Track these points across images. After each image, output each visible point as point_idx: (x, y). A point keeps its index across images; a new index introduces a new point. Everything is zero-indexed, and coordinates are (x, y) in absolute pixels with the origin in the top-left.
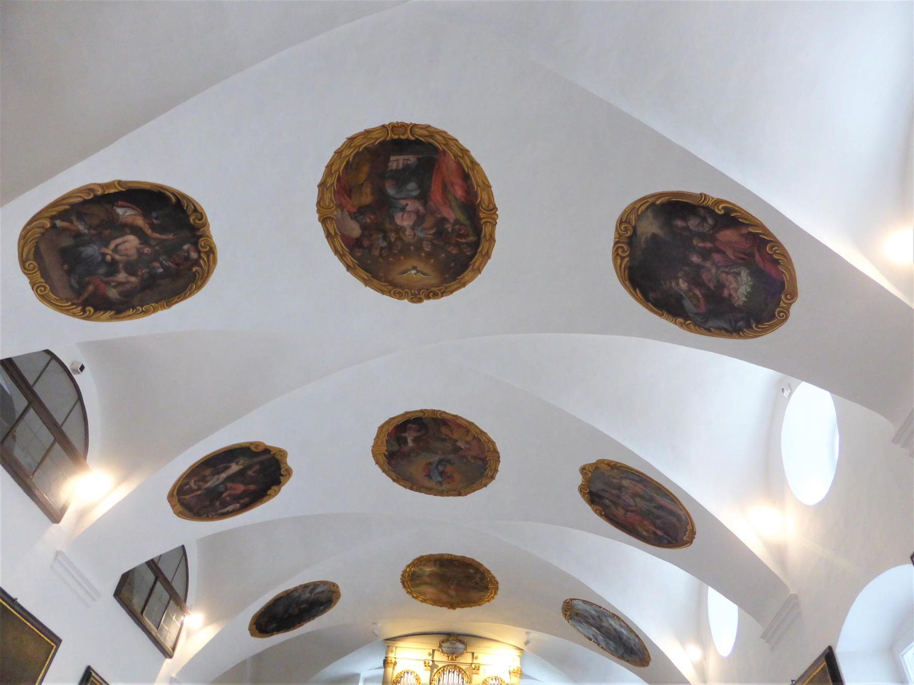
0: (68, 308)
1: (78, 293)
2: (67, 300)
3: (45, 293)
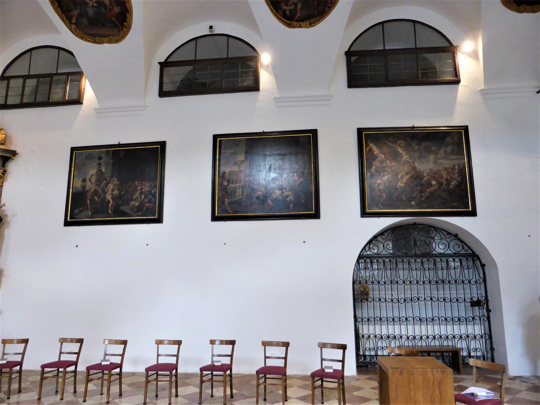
0: (124, 32)
1: (115, 26)
2: (119, 31)
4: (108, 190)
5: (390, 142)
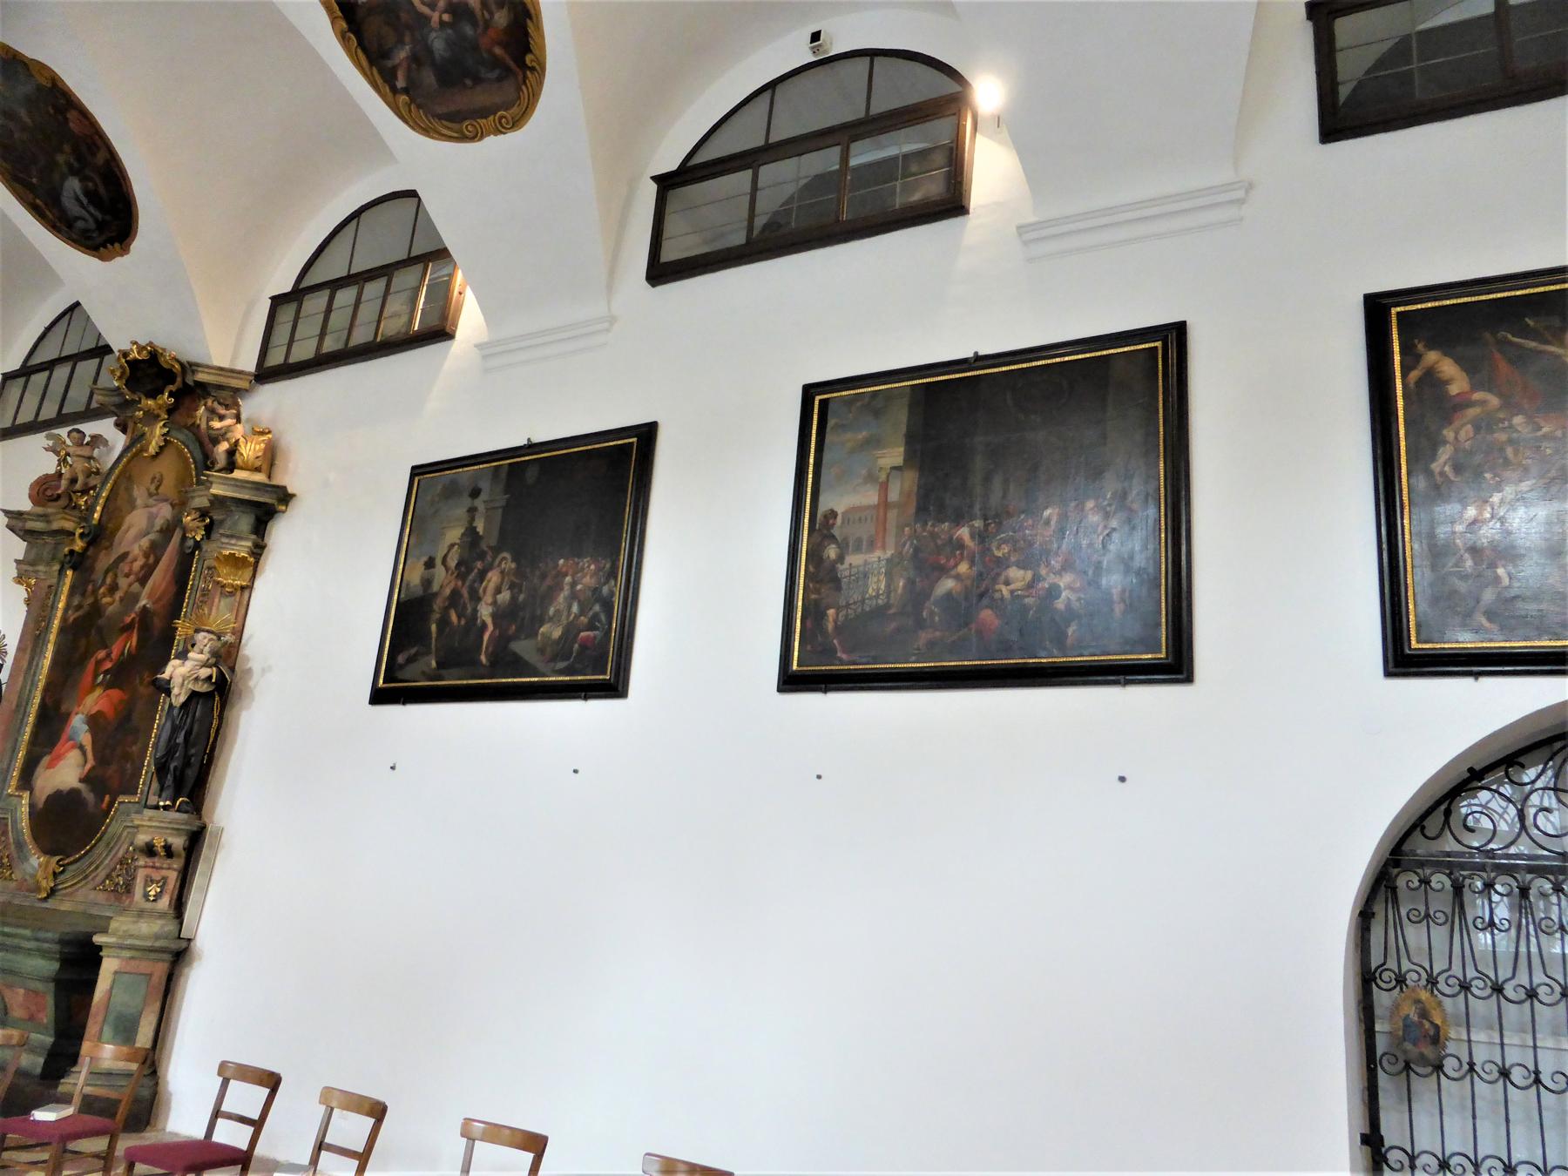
1: (508, 71)
2: (519, 89)
3: (510, 118)
4: (485, 591)
5: (1526, 333)
